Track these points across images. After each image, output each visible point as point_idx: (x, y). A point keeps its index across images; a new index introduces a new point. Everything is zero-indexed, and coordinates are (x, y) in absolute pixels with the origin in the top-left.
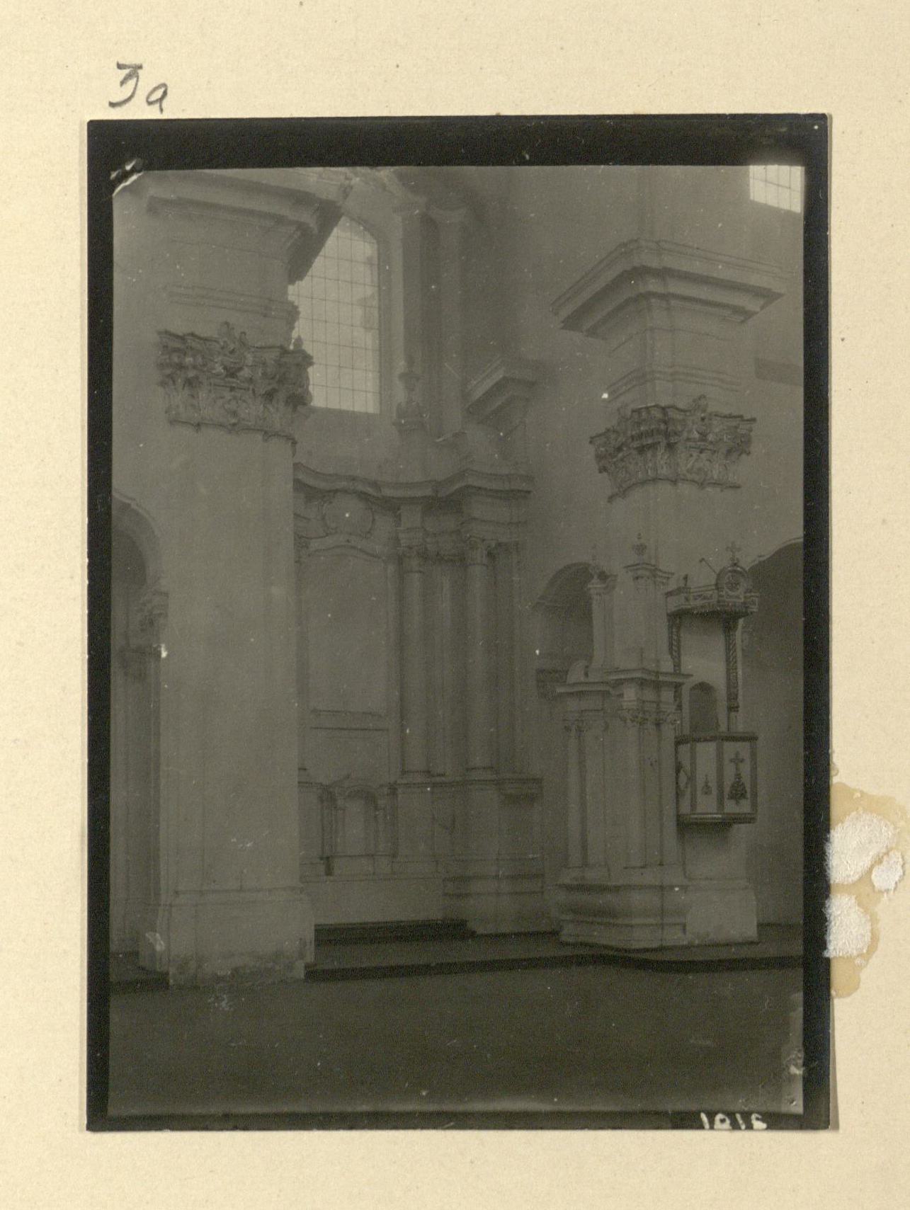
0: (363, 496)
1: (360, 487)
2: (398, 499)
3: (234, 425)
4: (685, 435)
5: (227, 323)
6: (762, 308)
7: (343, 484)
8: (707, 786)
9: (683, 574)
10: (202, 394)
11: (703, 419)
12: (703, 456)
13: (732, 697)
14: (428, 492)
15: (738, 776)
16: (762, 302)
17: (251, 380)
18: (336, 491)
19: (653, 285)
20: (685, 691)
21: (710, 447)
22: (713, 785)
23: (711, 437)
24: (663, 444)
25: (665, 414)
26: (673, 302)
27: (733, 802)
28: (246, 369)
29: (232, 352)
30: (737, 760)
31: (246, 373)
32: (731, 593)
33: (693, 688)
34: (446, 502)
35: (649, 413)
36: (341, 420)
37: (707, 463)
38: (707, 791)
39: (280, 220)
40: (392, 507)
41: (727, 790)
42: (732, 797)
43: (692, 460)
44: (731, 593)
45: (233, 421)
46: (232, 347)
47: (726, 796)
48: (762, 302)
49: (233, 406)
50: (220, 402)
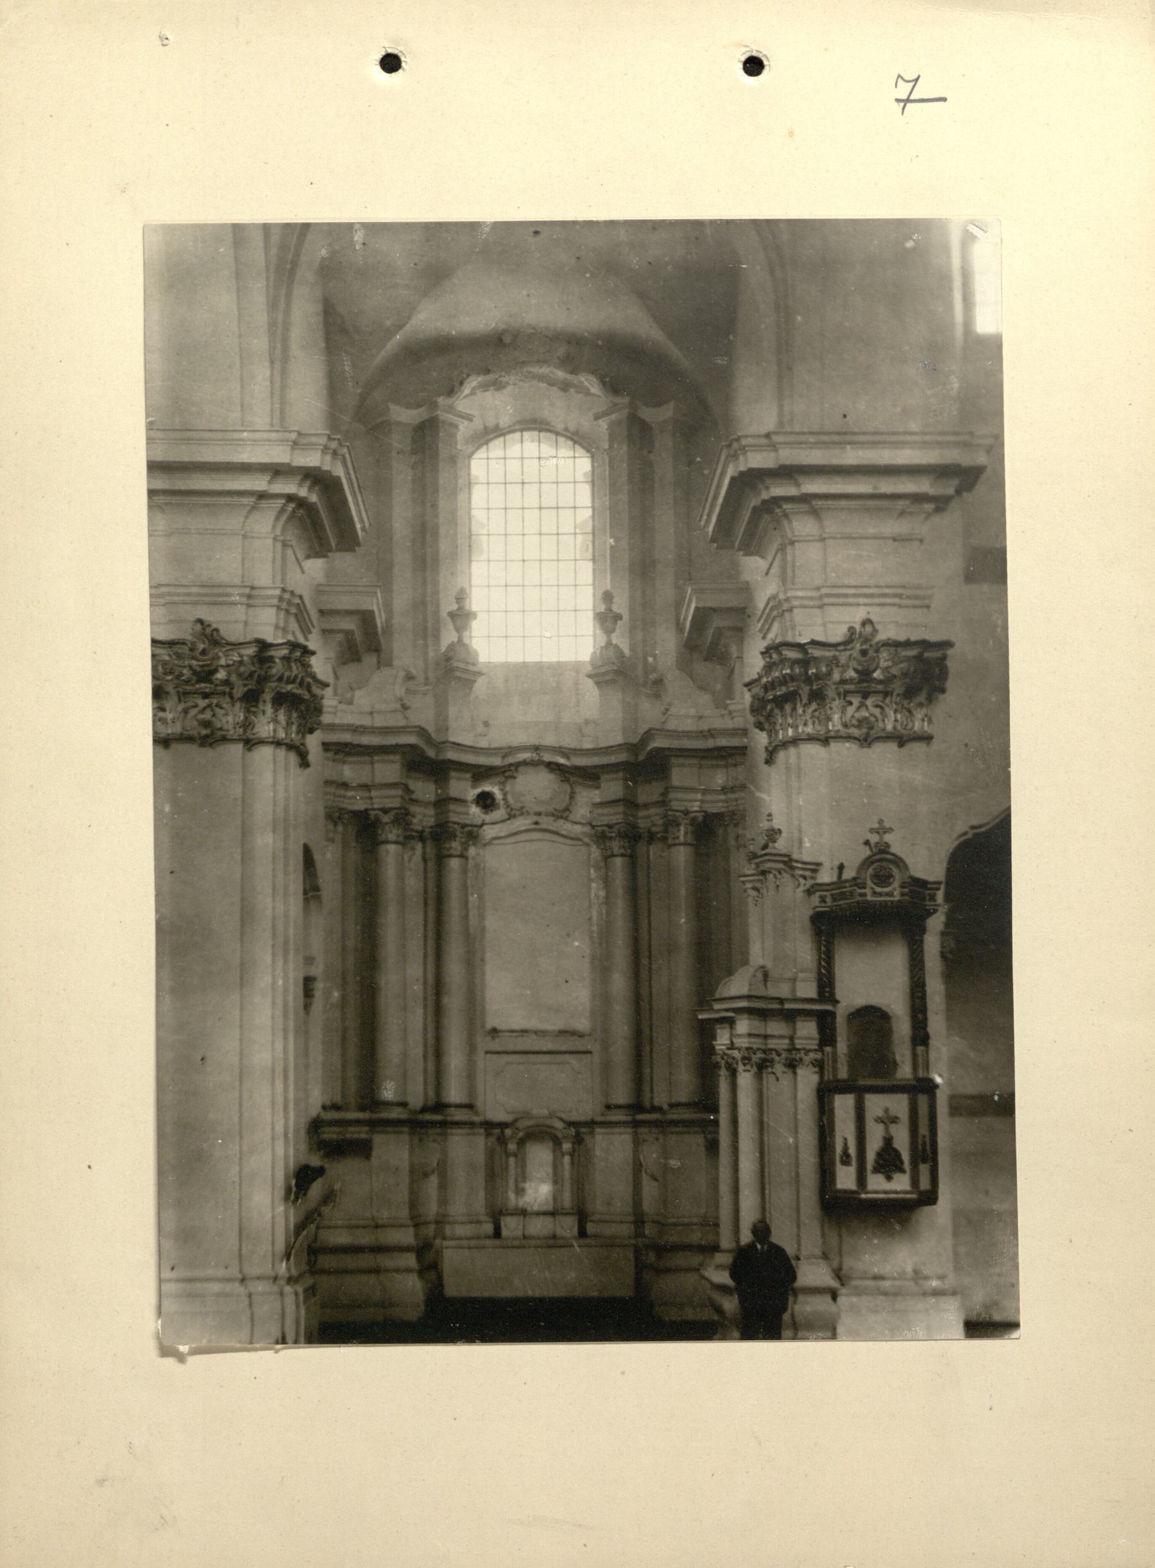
0: (552, 767)
3: (207, 736)
4: (836, 676)
5: (200, 621)
7: (526, 756)
9: (836, 863)
12: (869, 702)
15: (888, 1140)
17: (226, 682)
19: (778, 490)
21: (880, 687)
25: (806, 652)
28: (221, 670)
29: (203, 652)
32: (878, 890)
35: (780, 653)
37: (877, 711)
38: (846, 1161)
39: (262, 496)
40: (590, 776)
41: (871, 1156)
42: (877, 1170)
43: (851, 710)
45: (204, 732)
46: (201, 646)
47: (869, 1165)
49: (207, 715)
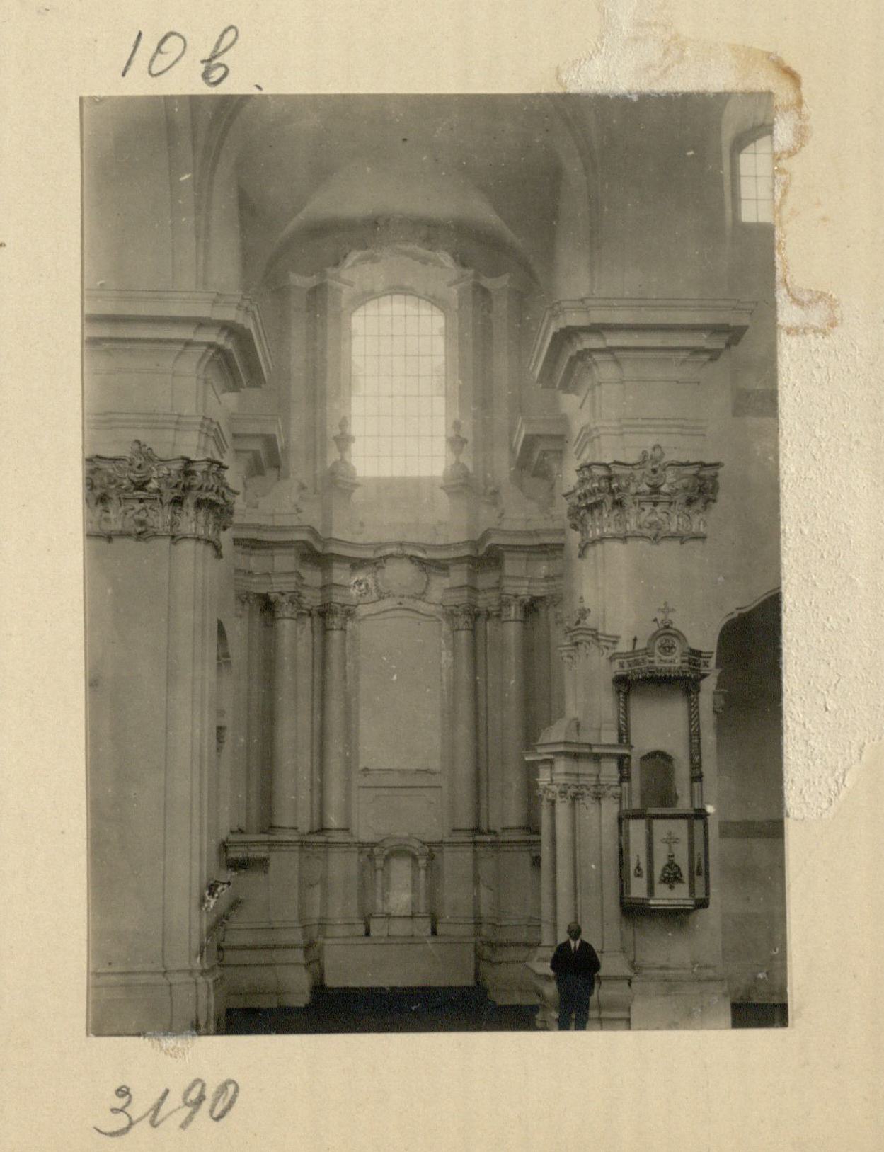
0: (412, 559)
1: (409, 552)
2: (503, 546)
4: (633, 489)
5: (138, 442)
6: (728, 345)
7: (394, 550)
8: (638, 867)
10: (112, 506)
11: (654, 471)
12: (658, 509)
13: (696, 765)
14: (466, 552)
16: (726, 337)
17: (158, 491)
18: (386, 557)
20: (635, 762)
21: (667, 498)
22: (644, 866)
23: (664, 488)
24: (609, 500)
25: (610, 470)
26: (618, 354)
27: (666, 886)
29: (139, 467)
30: (671, 840)
31: (153, 485)
32: (664, 658)
33: (643, 758)
34: (485, 558)
36: (403, 491)
39: (188, 343)
43: (644, 515)
44: (664, 658)
46: (138, 462)
48: (726, 337)
49: (142, 516)
50: (131, 513)
